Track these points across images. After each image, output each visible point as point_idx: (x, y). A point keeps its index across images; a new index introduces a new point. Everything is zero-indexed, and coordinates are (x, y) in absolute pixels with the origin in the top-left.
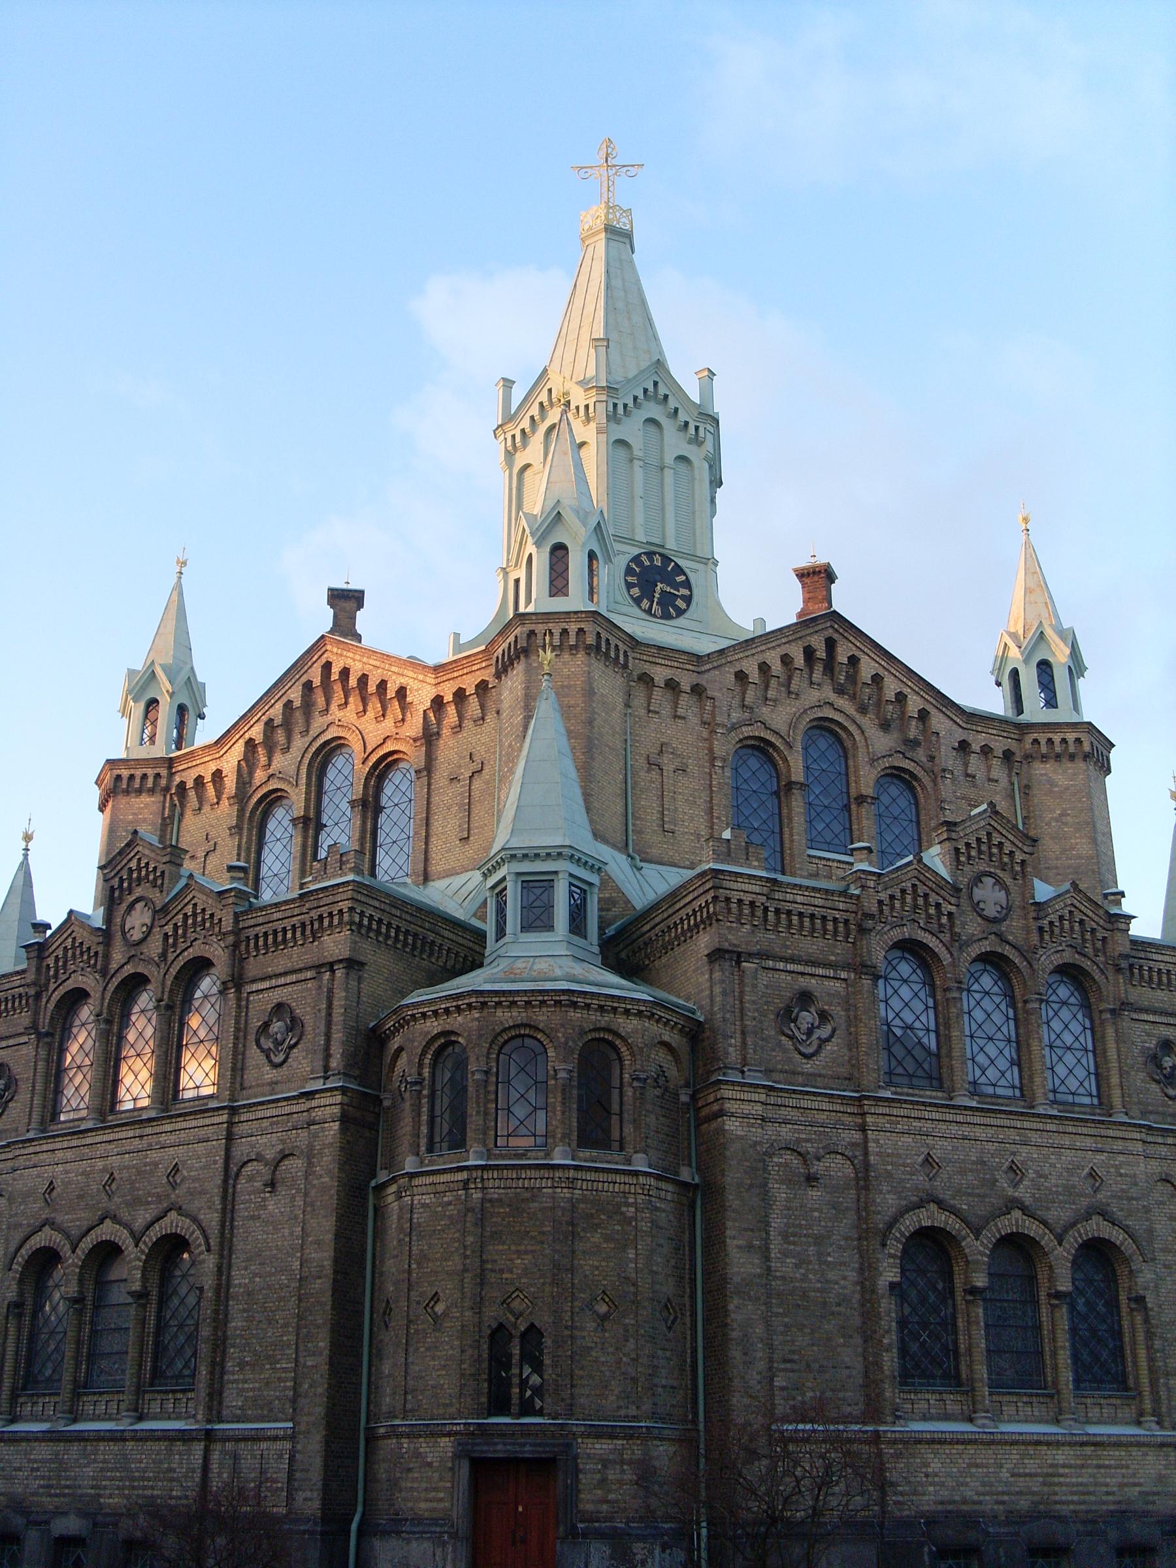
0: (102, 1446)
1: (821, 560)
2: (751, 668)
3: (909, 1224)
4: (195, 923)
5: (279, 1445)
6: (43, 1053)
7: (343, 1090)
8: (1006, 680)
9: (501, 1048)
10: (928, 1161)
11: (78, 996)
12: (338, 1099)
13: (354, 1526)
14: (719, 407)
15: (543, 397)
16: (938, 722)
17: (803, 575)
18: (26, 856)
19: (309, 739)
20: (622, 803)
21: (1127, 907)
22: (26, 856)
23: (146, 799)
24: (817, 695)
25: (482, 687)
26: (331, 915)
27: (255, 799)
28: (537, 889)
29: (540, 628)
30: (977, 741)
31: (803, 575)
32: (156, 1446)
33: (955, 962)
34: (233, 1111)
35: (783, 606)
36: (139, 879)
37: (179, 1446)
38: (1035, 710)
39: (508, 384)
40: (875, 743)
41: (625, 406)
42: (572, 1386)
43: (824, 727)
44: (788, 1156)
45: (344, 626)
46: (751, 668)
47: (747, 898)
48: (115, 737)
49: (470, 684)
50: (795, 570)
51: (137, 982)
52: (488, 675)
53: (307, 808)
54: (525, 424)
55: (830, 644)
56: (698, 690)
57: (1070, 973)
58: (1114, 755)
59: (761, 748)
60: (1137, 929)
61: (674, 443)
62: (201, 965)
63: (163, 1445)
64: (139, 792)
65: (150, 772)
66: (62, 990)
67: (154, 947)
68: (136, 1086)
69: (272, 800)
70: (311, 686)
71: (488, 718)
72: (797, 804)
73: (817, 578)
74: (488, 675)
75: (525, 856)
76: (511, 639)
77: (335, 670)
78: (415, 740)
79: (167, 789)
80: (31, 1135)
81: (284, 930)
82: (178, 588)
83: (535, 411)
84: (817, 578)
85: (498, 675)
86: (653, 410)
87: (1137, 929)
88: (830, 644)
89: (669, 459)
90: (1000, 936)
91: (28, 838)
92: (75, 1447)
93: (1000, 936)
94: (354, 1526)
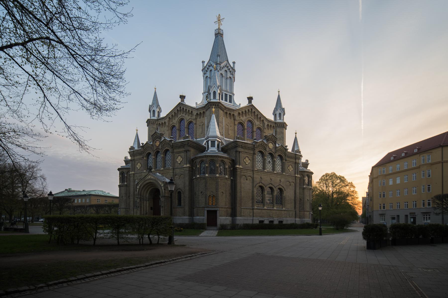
1: (251, 96)
2: (240, 112)
3: (258, 185)
9: (32, 76)
14: (236, 68)
16: (265, 122)
21: (288, 148)
24: (250, 117)
25: (204, 112)
28: (213, 143)
30: (270, 124)
33: (267, 153)
34: (173, 169)
35: (244, 103)
38: (278, 121)
39: (203, 62)
43: (250, 121)
45: (182, 100)
46: (240, 112)
48: (148, 116)
49: (202, 112)
54: (206, 69)
55: (252, 109)
56: (233, 115)
57: (261, 152)
58: (287, 127)
59: (241, 124)
61: (229, 75)
62: (167, 150)
67: (160, 147)
69: (174, 126)
70: (181, 108)
72: (255, 133)
73: (250, 99)
74: (205, 110)
82: (137, 134)
83: (208, 67)
84: (250, 99)
86: (226, 69)
87: (288, 150)
88: (252, 109)
89: (228, 77)
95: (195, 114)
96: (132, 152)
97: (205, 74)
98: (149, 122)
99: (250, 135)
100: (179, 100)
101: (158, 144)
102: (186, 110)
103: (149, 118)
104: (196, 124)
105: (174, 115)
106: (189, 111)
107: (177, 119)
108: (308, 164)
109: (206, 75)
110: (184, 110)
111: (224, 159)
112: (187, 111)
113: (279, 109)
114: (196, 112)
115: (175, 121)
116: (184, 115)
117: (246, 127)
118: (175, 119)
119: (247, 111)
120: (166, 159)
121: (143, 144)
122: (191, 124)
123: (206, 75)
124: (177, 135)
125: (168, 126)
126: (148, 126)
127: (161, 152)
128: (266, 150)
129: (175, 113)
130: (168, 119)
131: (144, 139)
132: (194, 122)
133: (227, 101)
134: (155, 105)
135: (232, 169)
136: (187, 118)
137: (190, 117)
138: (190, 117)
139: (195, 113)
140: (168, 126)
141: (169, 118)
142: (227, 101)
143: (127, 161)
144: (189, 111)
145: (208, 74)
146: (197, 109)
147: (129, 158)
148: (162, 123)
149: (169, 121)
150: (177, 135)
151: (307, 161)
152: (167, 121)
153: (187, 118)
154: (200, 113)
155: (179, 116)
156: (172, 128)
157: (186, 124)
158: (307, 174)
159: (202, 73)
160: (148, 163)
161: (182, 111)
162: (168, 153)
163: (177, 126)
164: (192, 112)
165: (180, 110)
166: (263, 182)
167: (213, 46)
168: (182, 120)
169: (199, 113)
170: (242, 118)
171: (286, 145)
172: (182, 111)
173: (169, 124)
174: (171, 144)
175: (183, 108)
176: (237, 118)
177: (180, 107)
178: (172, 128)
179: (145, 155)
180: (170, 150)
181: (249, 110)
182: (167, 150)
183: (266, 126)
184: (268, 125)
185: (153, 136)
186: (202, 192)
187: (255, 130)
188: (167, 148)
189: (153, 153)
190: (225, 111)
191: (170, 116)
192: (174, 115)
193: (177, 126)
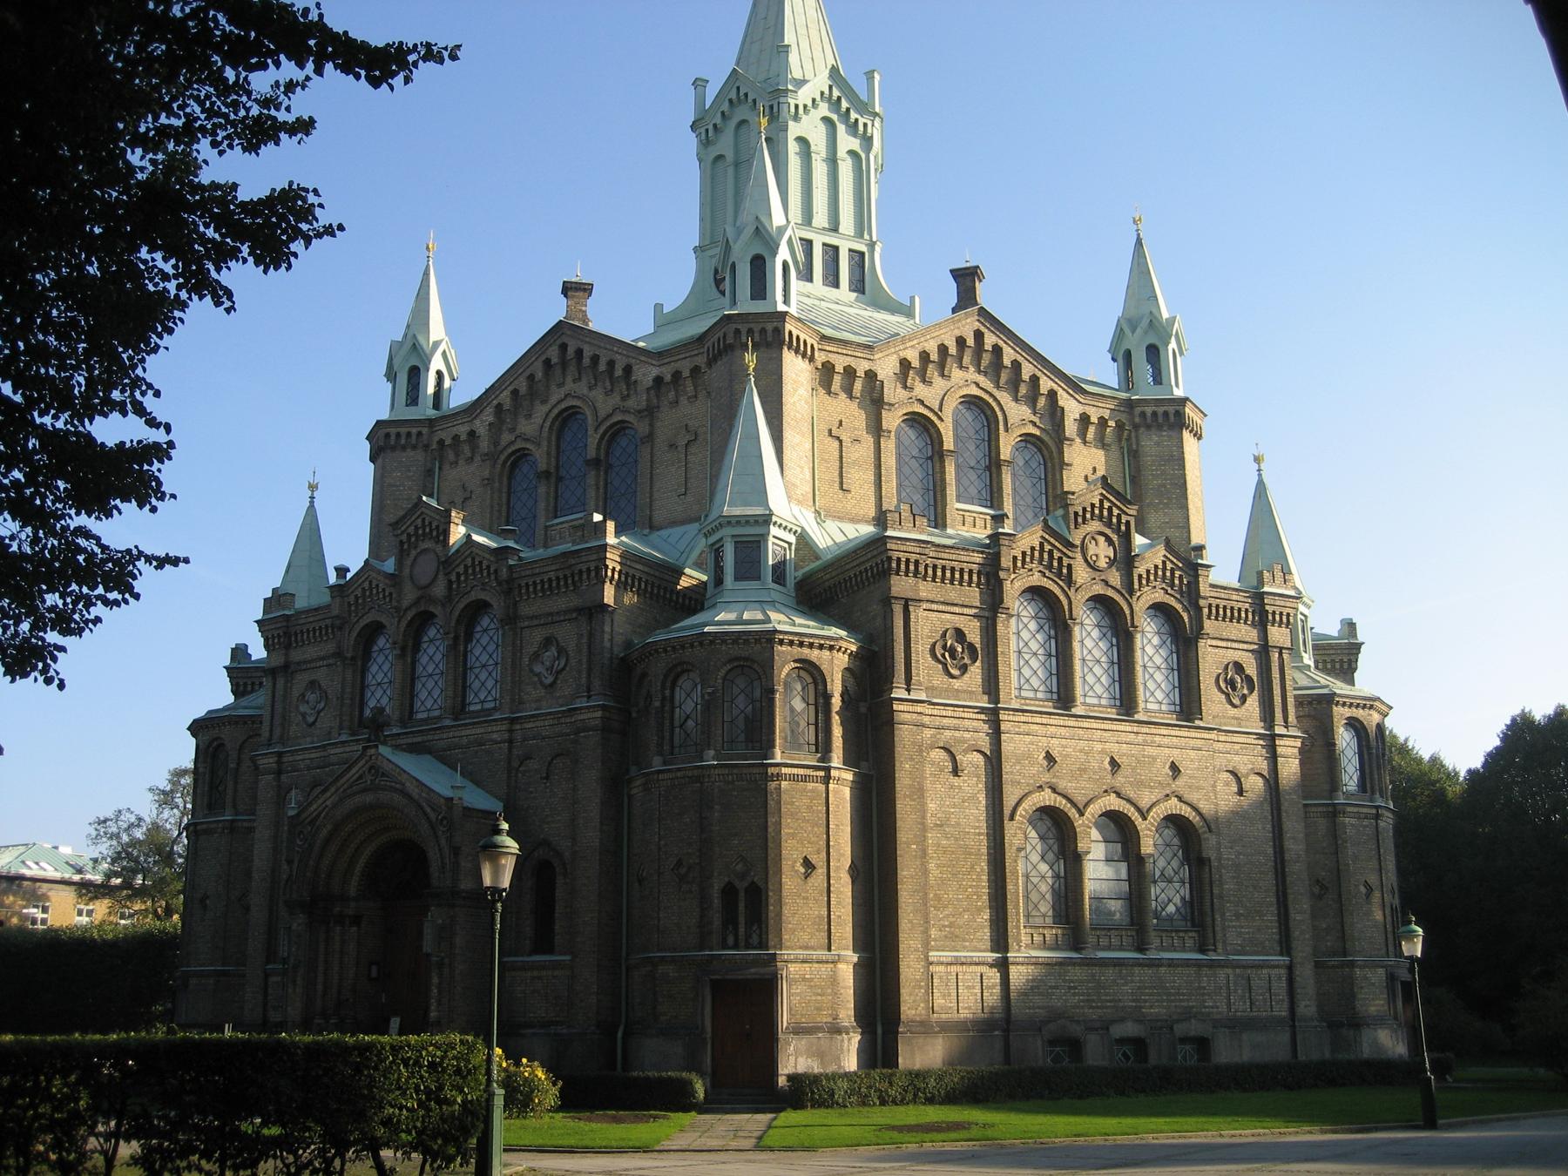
0: (1137, 970)
4: (474, 572)
5: (1276, 971)
6: (349, 676)
7: (603, 708)
8: (1120, 358)
10: (1049, 757)
11: (376, 629)
12: (599, 714)
13: (620, 1034)
15: (733, 95)
17: (958, 274)
18: (312, 502)
19: (548, 406)
20: (808, 446)
22: (312, 502)
23: (410, 453)
24: (965, 380)
25: (695, 370)
26: (589, 570)
27: (502, 458)
29: (744, 328)
31: (958, 274)
32: (1186, 971)
36: (424, 534)
37: (1205, 971)
38: (1146, 390)
39: (699, 84)
40: (1018, 416)
41: (805, 106)
42: (511, 741)
44: (943, 754)
47: (913, 557)
48: (379, 403)
49: (685, 367)
50: (952, 271)
51: (425, 619)
52: (701, 361)
53: (548, 464)
60: (1215, 576)
62: (480, 607)
63: (1192, 970)
64: (404, 448)
65: (414, 431)
66: (362, 623)
67: (439, 590)
68: (431, 697)
70: (567, 352)
71: (700, 396)
74: (701, 361)
75: (738, 523)
76: (721, 334)
77: (571, 351)
78: (639, 412)
79: (426, 446)
80: (344, 738)
81: (550, 580)
83: (725, 107)
85: (710, 364)
87: (1215, 576)
90: (1106, 583)
91: (313, 487)
92: (1110, 971)
93: (1106, 583)
94: (620, 1034)
95: (648, 381)
96: (280, 620)
97: (705, 143)
98: (384, 441)
99: (976, 483)
100: (555, 310)
101: (426, 568)
102: (595, 359)
103: (385, 416)
104: (650, 437)
105: (523, 390)
106: (611, 364)
107: (541, 410)
108: (1358, 647)
109: (714, 151)
110: (586, 361)
111: (814, 655)
112: (602, 367)
113: (1143, 343)
114: (655, 372)
115: (533, 423)
116: (581, 387)
117: (949, 444)
118: (528, 416)
119: (953, 350)
120: (471, 660)
121: (341, 571)
122: (623, 442)
123: (714, 151)
124: (542, 505)
125: (491, 457)
126: (373, 459)
127: (440, 621)
128: (1069, 580)
129: (531, 378)
130: (488, 416)
131: (348, 546)
132: (642, 428)
133: (836, 285)
134: (408, 367)
135: (863, 710)
136: (603, 402)
137: (615, 400)
138: (615, 400)
139: (646, 374)
140: (491, 457)
141: (499, 407)
142: (836, 285)
143: (241, 672)
144: (611, 364)
145: (725, 145)
146: (660, 355)
147: (258, 651)
148: (456, 438)
149: (496, 428)
150: (542, 505)
151: (1350, 626)
152: (481, 426)
153: (603, 402)
154: (677, 375)
155: (556, 395)
156: (514, 465)
157: (593, 440)
158: (1347, 712)
159: (692, 141)
160: (363, 687)
161: (572, 369)
162: (485, 622)
163: (541, 457)
164: (628, 370)
165: (564, 363)
166: (1062, 785)
167: (749, 25)
168: (567, 418)
169: (668, 378)
170: (920, 390)
171: (1196, 540)
172: (572, 369)
173: (496, 443)
174: (504, 572)
175: (579, 353)
176: (893, 392)
177: (564, 347)
178: (514, 465)
179: (350, 639)
180: (497, 603)
181: (961, 342)
182: (480, 607)
183: (1071, 428)
184: (1084, 420)
185: (401, 526)
186: (679, 863)
187: (1006, 452)
188: (477, 594)
189: (395, 628)
190: (820, 357)
191: (505, 397)
192: (523, 390)
193: (541, 457)
